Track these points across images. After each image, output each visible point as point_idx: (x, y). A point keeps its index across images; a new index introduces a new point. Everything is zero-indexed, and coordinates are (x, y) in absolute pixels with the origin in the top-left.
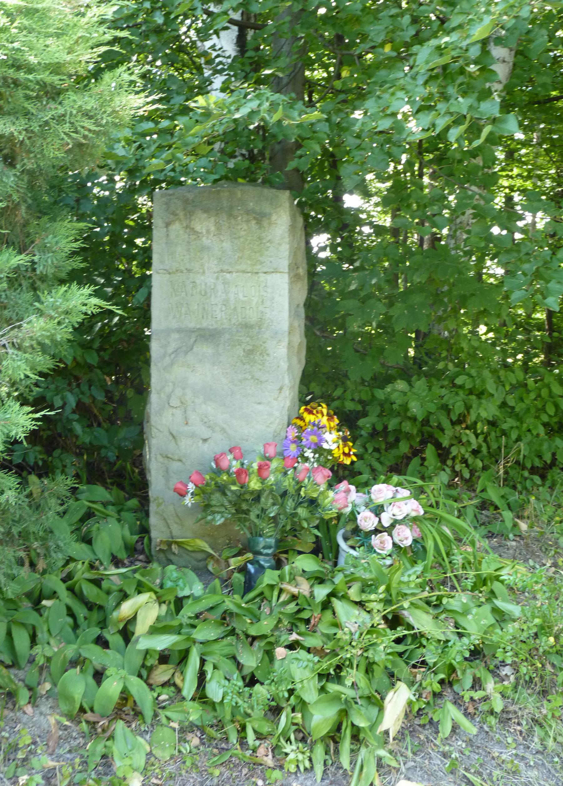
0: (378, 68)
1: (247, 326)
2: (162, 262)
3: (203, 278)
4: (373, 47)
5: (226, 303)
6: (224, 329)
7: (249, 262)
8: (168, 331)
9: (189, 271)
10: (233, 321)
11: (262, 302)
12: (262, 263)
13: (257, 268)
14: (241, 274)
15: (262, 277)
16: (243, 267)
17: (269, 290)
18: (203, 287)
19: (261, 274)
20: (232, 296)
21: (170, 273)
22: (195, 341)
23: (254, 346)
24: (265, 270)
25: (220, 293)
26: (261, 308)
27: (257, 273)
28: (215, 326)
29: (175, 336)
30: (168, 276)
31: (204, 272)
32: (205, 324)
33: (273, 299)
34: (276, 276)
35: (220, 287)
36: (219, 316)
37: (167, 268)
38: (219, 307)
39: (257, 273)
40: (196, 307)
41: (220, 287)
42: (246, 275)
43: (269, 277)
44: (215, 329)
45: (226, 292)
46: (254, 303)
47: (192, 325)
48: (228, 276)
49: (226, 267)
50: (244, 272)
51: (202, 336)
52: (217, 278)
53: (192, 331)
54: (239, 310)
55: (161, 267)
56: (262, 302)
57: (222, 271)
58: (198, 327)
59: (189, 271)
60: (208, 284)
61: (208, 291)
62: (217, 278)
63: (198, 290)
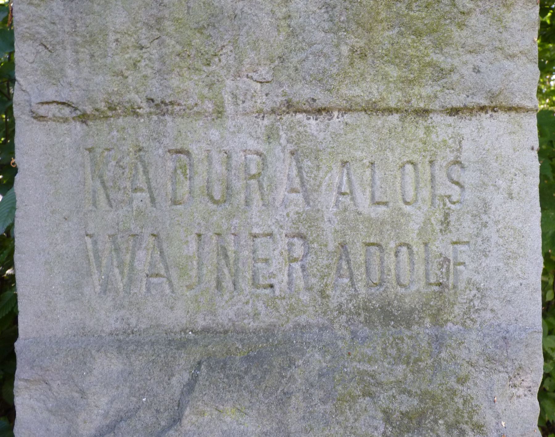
0: (132, 265)
1: (388, 315)
2: (52, 75)
3: (214, 134)
4: (154, 248)
5: (304, 232)
6: (301, 328)
7: (393, 72)
8: (82, 346)
9: (161, 107)
10: (336, 297)
11: (446, 221)
12: (441, 73)
13: (424, 92)
14: (364, 117)
15: (443, 127)
16: (369, 90)
17: (469, 177)
18: (219, 168)
19: (437, 118)
20: (327, 201)
21: (84, 118)
22: (190, 387)
23: (424, 396)
24: (456, 101)
25: (282, 193)
26: (441, 246)
27: (424, 112)
28: (267, 318)
29: (109, 365)
30: (78, 127)
31: (220, 112)
32: (226, 314)
33: (486, 207)
34: (495, 125)
35: (283, 168)
36: (281, 281)
37: (73, 97)
38: (283, 243)
39: (424, 112)
40: (193, 246)
41: (283, 168)
42: (379, 121)
43: (467, 127)
44: (269, 331)
45: (306, 189)
46: (414, 226)
47: (176, 317)
48: (312, 124)
49: (304, 92)
50: (373, 109)
51: (223, 365)
52: (271, 135)
53: (177, 342)
54: (358, 254)
55: (50, 94)
56: (446, 221)
57: (291, 107)
58: (201, 323)
59: (161, 107)
60: (238, 158)
61: (238, 184)
62: (271, 135)
63: (199, 181)
